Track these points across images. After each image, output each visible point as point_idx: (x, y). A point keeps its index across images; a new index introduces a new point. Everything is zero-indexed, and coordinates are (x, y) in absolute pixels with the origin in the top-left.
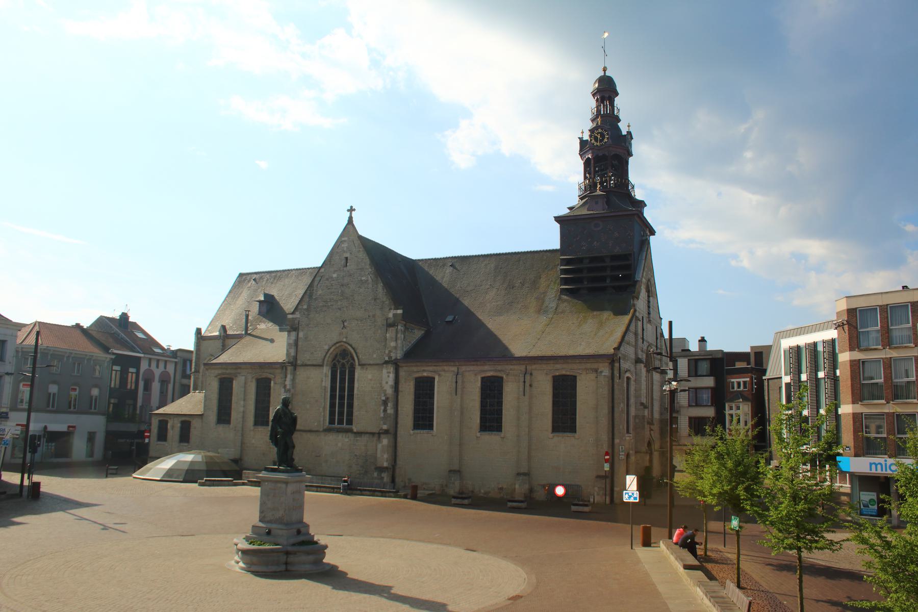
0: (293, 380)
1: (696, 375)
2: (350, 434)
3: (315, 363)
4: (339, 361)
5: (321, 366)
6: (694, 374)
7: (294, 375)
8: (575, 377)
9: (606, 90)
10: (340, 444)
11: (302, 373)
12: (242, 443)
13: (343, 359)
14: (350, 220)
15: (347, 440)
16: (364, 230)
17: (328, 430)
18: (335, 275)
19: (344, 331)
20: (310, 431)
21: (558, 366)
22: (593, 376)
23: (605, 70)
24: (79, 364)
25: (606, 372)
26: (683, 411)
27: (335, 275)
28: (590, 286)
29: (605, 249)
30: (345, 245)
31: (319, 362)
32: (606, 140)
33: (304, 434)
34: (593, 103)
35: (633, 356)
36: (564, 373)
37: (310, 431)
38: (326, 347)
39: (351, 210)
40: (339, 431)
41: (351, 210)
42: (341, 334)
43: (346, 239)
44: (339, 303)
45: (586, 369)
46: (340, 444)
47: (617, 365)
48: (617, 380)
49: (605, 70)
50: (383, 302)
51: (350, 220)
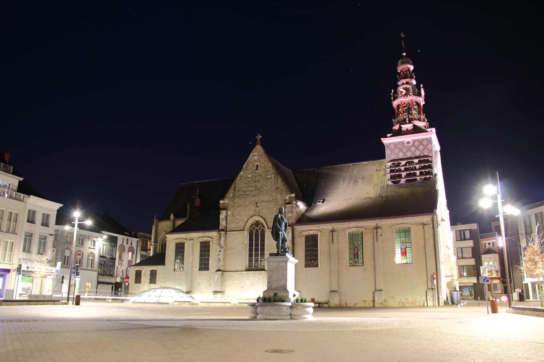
13: (257, 226)
18: (250, 176)
19: (258, 208)
27: (250, 176)
42: (255, 210)
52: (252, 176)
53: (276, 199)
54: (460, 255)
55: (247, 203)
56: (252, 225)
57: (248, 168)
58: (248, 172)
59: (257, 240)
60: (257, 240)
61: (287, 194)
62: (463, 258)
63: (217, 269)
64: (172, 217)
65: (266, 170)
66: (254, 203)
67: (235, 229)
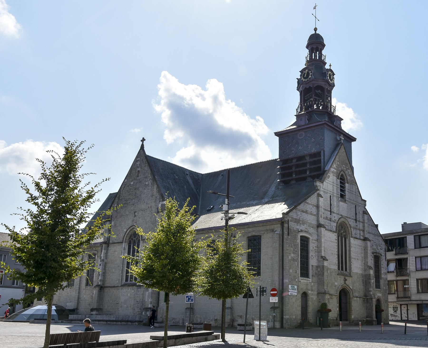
0: (106, 254)
1: (420, 247)
2: (135, 287)
3: (119, 241)
4: (132, 239)
5: (122, 243)
6: (418, 246)
7: (107, 250)
8: (261, 236)
9: (316, 43)
10: (129, 295)
11: (112, 249)
12: (79, 298)
13: (135, 237)
14: (142, 147)
15: (133, 291)
16: (149, 152)
17: (123, 286)
18: (132, 183)
19: (135, 218)
20: (114, 287)
21: (250, 230)
22: (270, 235)
23: (316, 29)
24: (5, 256)
25: (278, 230)
26: (412, 275)
27: (132, 183)
28: (297, 177)
29: (313, 150)
30: (138, 163)
31: (121, 240)
32: (310, 77)
33: (111, 289)
34: (306, 52)
35: (315, 223)
36: (254, 234)
37: (114, 287)
38: (125, 230)
39: (143, 140)
40: (129, 285)
41: (143, 140)
42: (133, 220)
43: (139, 159)
44: (133, 201)
45: (267, 230)
46: (129, 295)
47: (286, 225)
48: (285, 236)
49: (316, 29)
50: (156, 197)
51: (142, 147)
52: (134, 183)
53: (151, 206)
54: (419, 266)
55: (127, 213)
56: (131, 236)
57: (131, 175)
58: (131, 179)
59: (342, 240)
60: (342, 240)
61: (160, 201)
62: (422, 269)
63: (272, 288)
64: (225, 207)
65: (145, 176)
66: (133, 212)
67: (116, 241)
